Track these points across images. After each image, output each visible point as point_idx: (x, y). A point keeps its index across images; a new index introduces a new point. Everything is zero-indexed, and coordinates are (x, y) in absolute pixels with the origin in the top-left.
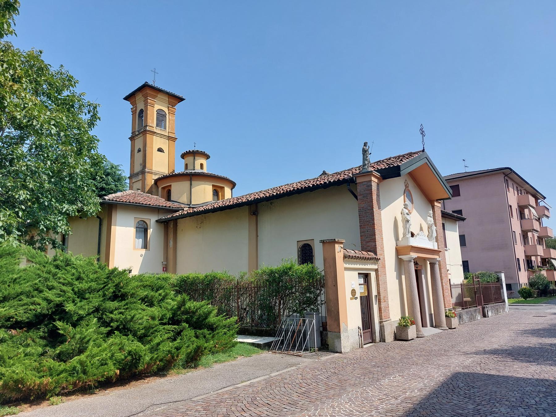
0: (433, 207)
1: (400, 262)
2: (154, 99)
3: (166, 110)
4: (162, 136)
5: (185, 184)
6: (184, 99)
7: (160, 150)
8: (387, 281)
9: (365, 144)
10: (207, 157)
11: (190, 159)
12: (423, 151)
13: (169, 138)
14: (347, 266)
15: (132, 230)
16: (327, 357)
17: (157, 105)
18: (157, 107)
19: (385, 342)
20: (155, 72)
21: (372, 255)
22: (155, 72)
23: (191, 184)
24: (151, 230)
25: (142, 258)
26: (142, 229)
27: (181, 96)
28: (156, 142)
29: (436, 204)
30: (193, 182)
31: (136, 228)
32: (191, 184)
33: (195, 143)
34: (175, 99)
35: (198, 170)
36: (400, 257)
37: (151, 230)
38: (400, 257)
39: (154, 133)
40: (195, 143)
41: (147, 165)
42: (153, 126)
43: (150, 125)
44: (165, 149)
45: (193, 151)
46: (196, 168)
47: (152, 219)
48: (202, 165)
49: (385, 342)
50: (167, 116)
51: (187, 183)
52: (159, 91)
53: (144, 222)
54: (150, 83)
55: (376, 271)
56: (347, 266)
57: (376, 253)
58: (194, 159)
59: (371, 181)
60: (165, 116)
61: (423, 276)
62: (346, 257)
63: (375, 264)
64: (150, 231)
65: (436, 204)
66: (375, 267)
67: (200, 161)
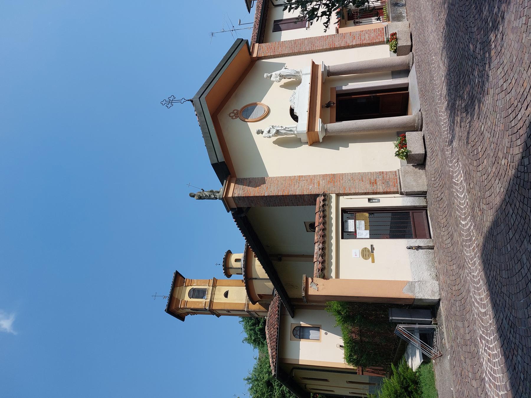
0: (259, 58)
1: (330, 140)
2: (179, 301)
3: (188, 289)
4: (213, 294)
5: (255, 283)
6: (177, 271)
7: (226, 295)
8: (351, 172)
9: (193, 196)
10: (229, 253)
11: (231, 271)
12: (192, 101)
13: (214, 286)
14: (333, 274)
15: (303, 343)
16: (442, 308)
17: (186, 299)
18: (187, 298)
19: (426, 192)
20: (155, 296)
21: (320, 200)
22: (155, 296)
23: (256, 279)
24: (301, 323)
25: (329, 333)
26: (301, 333)
27: (173, 275)
28: (219, 299)
29: (255, 55)
30: (254, 276)
31: (300, 338)
32: (256, 279)
33: (217, 264)
34: (178, 279)
35: (240, 265)
36: (321, 140)
37: (301, 323)
38: (321, 140)
39: (211, 302)
40: (217, 264)
41: (241, 308)
42: (204, 302)
43: (204, 305)
44: (224, 289)
45: (223, 266)
46: (240, 267)
47: (292, 322)
48: (237, 260)
49: (426, 192)
50: (194, 287)
51: (255, 282)
52: (172, 298)
53: (294, 329)
54: (165, 307)
55: (338, 195)
56: (333, 274)
57: (317, 195)
58: (231, 268)
59: (233, 198)
60: (194, 290)
61: (344, 88)
62: (324, 274)
63: (331, 198)
64: (303, 324)
65: (255, 55)
66: (334, 196)
67: (233, 263)
